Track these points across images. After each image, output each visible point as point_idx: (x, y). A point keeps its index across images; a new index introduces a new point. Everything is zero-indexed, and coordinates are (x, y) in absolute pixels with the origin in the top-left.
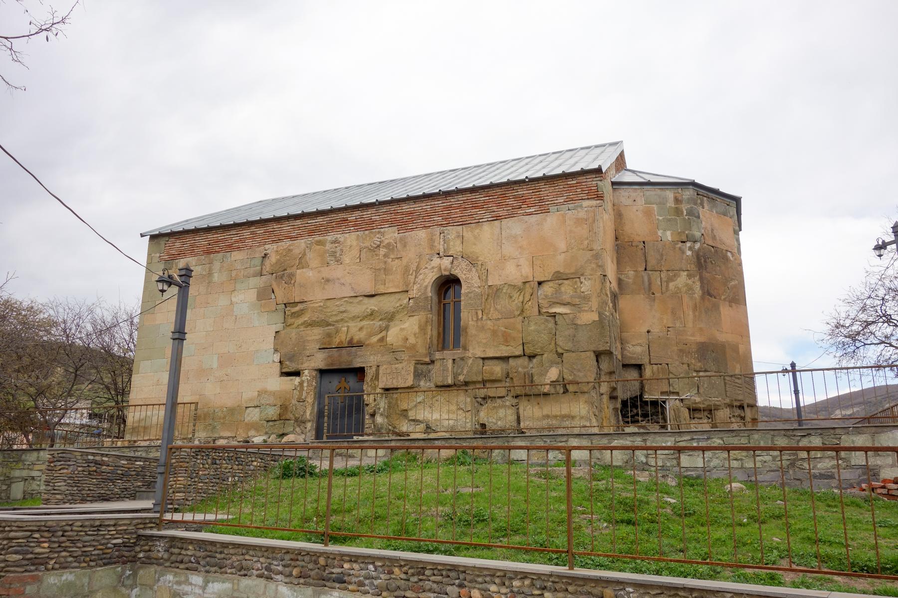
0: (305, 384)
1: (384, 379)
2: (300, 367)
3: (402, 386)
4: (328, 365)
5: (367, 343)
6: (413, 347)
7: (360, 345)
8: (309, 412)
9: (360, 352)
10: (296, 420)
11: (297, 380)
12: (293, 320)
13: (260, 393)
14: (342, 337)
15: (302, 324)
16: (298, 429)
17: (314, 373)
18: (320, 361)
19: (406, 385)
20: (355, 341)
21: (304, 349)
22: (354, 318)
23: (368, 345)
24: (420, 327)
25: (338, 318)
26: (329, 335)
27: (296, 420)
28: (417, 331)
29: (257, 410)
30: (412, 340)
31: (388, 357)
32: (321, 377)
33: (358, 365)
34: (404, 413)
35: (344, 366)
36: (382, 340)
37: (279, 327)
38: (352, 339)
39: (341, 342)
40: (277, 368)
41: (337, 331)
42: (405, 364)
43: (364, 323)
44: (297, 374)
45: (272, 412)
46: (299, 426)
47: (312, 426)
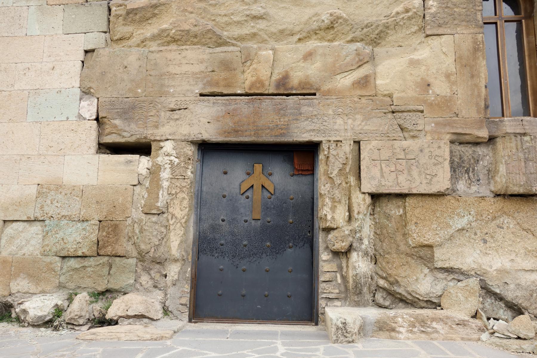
0: (165, 174)
1: (376, 172)
3: (423, 190)
4: (228, 133)
5: (326, 87)
6: (445, 103)
7: (308, 93)
8: (178, 240)
9: (308, 107)
10: (142, 257)
11: (143, 163)
12: (129, 29)
13: (43, 190)
14: (262, 70)
15: (154, 38)
16: (144, 279)
17: (190, 150)
18: (206, 122)
19: (433, 190)
21: (163, 94)
22: (283, 34)
23: (328, 93)
24: (458, 59)
25: (245, 31)
26: (226, 65)
27: (142, 257)
28: (453, 69)
29: (36, 228)
30: (440, 88)
31: (385, 123)
33: (305, 137)
34: (424, 254)
35: (267, 138)
36: (365, 82)
37: (95, 40)
40: (89, 134)
41: (248, 58)
42: (424, 141)
43: (312, 44)
44: (143, 149)
45: (77, 237)
46: (147, 270)
47: (181, 272)
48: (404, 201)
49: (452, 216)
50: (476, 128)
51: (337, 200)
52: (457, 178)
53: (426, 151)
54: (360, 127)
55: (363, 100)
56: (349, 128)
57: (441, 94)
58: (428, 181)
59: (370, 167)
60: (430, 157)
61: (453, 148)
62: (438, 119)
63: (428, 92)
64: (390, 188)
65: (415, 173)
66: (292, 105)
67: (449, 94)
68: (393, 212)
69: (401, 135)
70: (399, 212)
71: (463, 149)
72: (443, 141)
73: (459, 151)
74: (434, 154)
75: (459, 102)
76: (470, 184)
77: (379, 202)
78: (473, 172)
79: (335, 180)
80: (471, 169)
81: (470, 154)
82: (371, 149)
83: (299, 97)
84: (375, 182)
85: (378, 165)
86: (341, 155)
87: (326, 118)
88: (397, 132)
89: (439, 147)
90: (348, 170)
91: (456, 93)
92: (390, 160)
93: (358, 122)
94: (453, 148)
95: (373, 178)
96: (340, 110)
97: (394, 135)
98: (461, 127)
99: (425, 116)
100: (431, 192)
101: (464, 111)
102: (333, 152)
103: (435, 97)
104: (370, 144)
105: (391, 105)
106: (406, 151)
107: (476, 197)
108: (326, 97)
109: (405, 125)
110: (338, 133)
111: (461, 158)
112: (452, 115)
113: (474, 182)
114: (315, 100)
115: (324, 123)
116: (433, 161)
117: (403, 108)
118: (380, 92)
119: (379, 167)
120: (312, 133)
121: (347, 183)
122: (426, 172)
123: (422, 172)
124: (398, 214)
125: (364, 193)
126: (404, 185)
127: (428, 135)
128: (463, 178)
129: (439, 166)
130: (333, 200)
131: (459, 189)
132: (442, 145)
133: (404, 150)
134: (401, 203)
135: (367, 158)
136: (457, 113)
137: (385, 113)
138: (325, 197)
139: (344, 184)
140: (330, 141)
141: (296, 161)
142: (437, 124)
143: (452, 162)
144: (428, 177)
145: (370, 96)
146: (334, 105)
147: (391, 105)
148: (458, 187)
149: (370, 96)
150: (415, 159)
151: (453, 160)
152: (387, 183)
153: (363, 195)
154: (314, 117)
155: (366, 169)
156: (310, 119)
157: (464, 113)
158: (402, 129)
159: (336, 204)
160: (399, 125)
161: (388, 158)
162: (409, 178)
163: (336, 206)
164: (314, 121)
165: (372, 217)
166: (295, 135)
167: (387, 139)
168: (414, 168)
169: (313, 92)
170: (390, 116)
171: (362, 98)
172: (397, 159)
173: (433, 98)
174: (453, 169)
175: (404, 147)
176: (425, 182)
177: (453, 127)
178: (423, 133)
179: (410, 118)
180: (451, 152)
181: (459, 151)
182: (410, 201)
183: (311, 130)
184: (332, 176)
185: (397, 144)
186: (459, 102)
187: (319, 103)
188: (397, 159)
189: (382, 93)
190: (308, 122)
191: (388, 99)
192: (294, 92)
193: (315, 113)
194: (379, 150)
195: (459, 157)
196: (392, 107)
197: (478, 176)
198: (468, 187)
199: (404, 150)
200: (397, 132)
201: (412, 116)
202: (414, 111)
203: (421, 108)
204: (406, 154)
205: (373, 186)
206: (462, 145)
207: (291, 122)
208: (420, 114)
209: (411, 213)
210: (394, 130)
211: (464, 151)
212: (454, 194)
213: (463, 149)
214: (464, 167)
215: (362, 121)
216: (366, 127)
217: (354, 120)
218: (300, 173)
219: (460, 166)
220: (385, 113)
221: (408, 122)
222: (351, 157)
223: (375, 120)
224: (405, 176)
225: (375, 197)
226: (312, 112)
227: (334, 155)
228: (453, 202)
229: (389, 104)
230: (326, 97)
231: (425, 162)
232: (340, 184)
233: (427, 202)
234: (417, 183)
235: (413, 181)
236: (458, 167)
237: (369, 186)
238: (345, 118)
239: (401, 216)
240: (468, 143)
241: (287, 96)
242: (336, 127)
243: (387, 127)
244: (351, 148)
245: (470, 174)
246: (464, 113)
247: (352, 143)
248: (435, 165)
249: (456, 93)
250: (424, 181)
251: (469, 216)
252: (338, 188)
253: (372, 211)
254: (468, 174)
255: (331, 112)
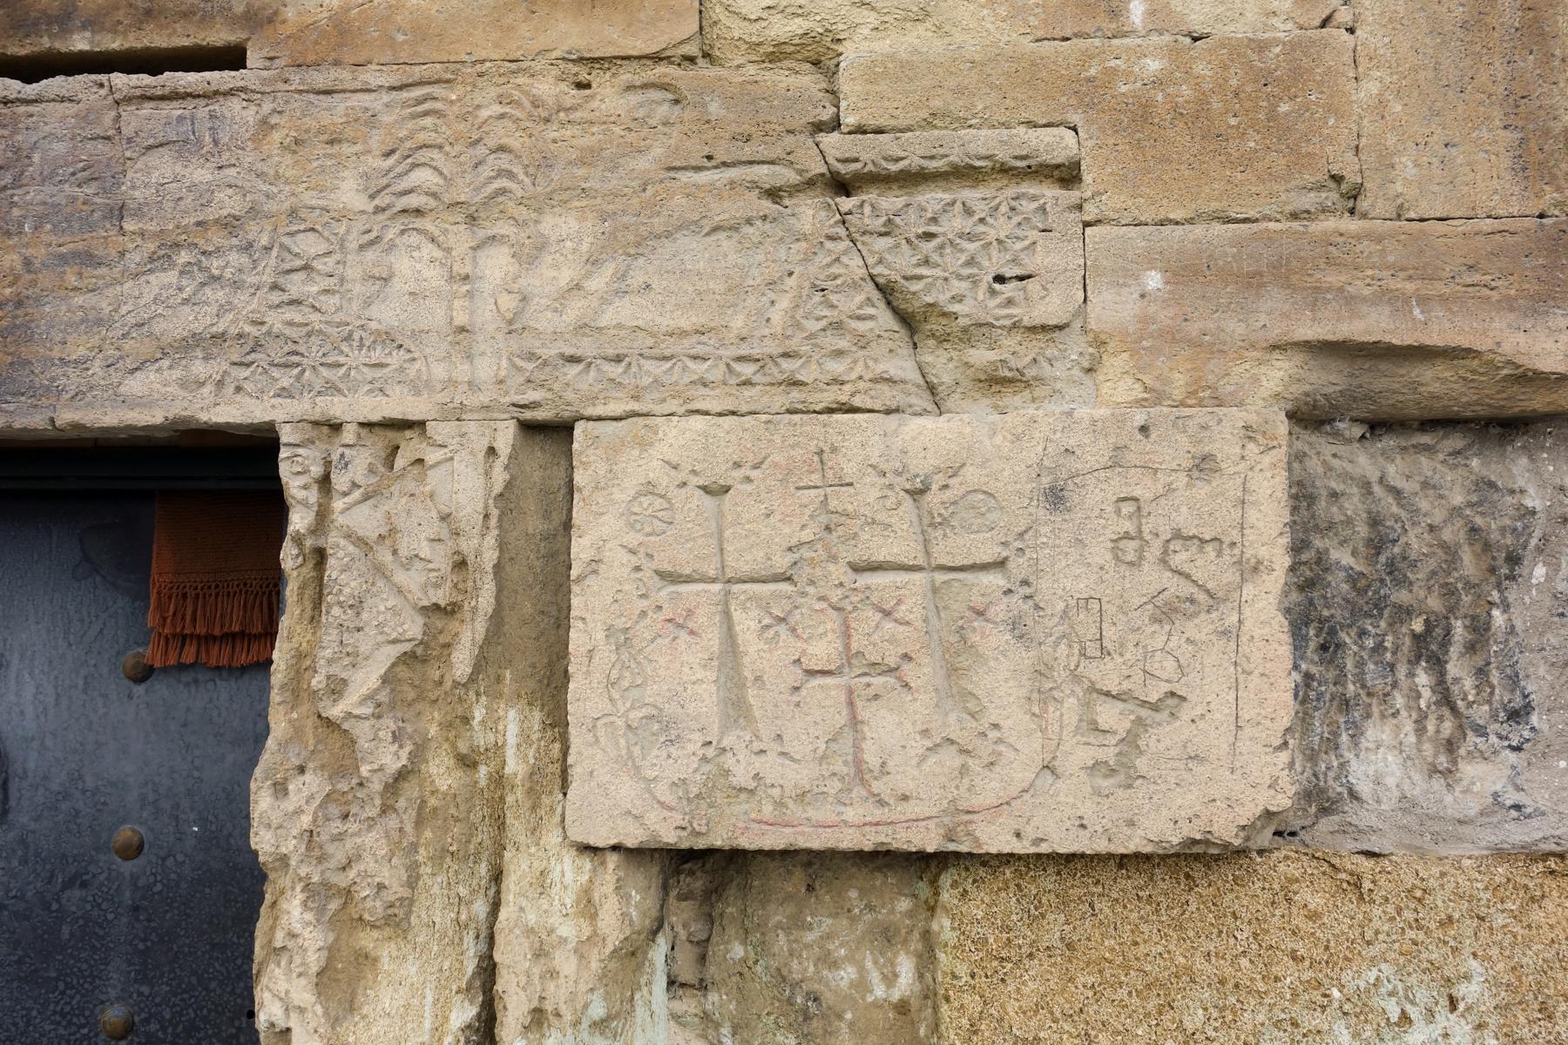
1: (684, 674)
19: (1157, 828)
42: (1083, 409)
48: (923, 889)
49: (1311, 1021)
50: (1509, 304)
51: (376, 908)
52: (1345, 704)
53: (1097, 496)
54: (575, 310)
55: (608, 96)
56: (486, 316)
57: (1220, 31)
58: (1109, 754)
59: (643, 631)
60: (1129, 549)
61: (1314, 465)
62: (1198, 230)
63: (1114, 14)
64: (795, 811)
65: (1001, 679)
66: (60, 148)
67: (1283, 29)
68: (848, 974)
69: (902, 365)
70: (890, 979)
71: (1395, 471)
72: (1238, 416)
73: (1366, 486)
74: (1158, 523)
75: (1370, 87)
76: (1450, 746)
77: (745, 889)
78: (1471, 648)
79: (364, 744)
80: (1459, 628)
81: (1456, 511)
82: (650, 489)
83: (119, 79)
84: (677, 765)
85: (701, 619)
86: (419, 536)
87: (309, 245)
88: (862, 342)
89: (1204, 465)
90: (462, 662)
91: (1344, 15)
92: (802, 574)
93: (556, 273)
94: (1314, 465)
95: (663, 727)
96: (422, 177)
97: (837, 367)
98: (1385, 296)
99: (1091, 212)
100: (1133, 843)
101: (1406, 166)
102: (360, 518)
103: (1174, 52)
104: (644, 445)
105: (818, 127)
106: (933, 498)
107: (1500, 854)
108: (320, 79)
109: (922, 293)
110: (397, 358)
111: (1377, 544)
112: (1308, 201)
113: (1481, 731)
114: (235, 104)
115: (297, 285)
116: (1152, 578)
117: (912, 151)
118: (738, 29)
119: (712, 639)
120: (199, 368)
121: (467, 762)
122: (1092, 671)
123: (1060, 675)
124: (879, 991)
125: (588, 849)
126: (906, 784)
127: (1115, 363)
128: (1399, 700)
129: (1201, 627)
130: (337, 904)
131: (1364, 788)
132: (1225, 444)
133: (917, 493)
134: (904, 904)
135: (618, 562)
136: (1352, 178)
137: (773, 194)
138: (285, 882)
139: (441, 773)
140: (336, 427)
141: (161, 572)
142: (1187, 273)
143: (1308, 577)
144: (1110, 715)
145: (657, 58)
146: (377, 140)
147: (818, 127)
148: (1360, 773)
149: (657, 58)
150: (1001, 564)
151: (1321, 559)
152: (771, 767)
153: (587, 863)
154: (217, 238)
155: (605, 655)
156: (184, 257)
157: (1408, 178)
158: (908, 321)
159: (367, 940)
160: (886, 291)
161: (781, 562)
162: (954, 724)
163: (365, 960)
164: (215, 264)
165: (688, 1005)
166: (72, 380)
167: (780, 400)
168: (993, 639)
169: (219, 36)
170: (810, 213)
171: (597, 78)
172: (857, 569)
173: (1153, 65)
174: (1316, 624)
175: (921, 465)
176: (1086, 755)
177: (1316, 297)
178: (1075, 346)
179: (968, 225)
180: (1302, 496)
181: (1366, 486)
182: (965, 911)
183: (191, 344)
184: (335, 711)
185: (861, 441)
186: (1370, 87)
187: (265, 126)
188: (857, 569)
189: (751, 32)
190: (171, 277)
191: (809, 81)
192: (80, 43)
193: (229, 203)
194: (717, 491)
195: (1363, 530)
196: (830, 140)
197: (1514, 681)
198: (1434, 770)
199: (917, 493)
200: (862, 342)
201: (981, 209)
202: (1004, 170)
203: (1057, 145)
204: (932, 524)
205: (663, 792)
206: (1389, 442)
207: (46, 279)
208: (1049, 192)
209: (972, 1003)
210: (837, 326)
211: (1408, 487)
212: (1326, 824)
213: (1395, 471)
214: (1404, 613)
215: (594, 262)
216: (623, 312)
217: (531, 254)
218: (189, 655)
219: (1368, 600)
220: (773, 194)
221: (955, 261)
222: (490, 556)
223: (693, 250)
224: (920, 707)
225: (703, 878)
226: (204, 196)
227: (361, 542)
228: (1316, 901)
229: (799, 122)
230: (320, 79)
231: (1082, 587)
232: (402, 776)
233: (1102, 906)
234: (1019, 770)
235: (984, 749)
236: (1355, 612)
237: (628, 790)
238: (460, 238)
239: (902, 1008)
240: (1440, 423)
241: (28, 80)
242: (386, 314)
243: (784, 303)
244: (500, 477)
245: (1453, 669)
246: (1408, 178)
247: (506, 436)
248: (1166, 612)
249: (1344, 15)
250: (1078, 755)
251: (1444, 1019)
252: (385, 810)
253: (686, 956)
254: (1438, 664)
255: (349, 194)
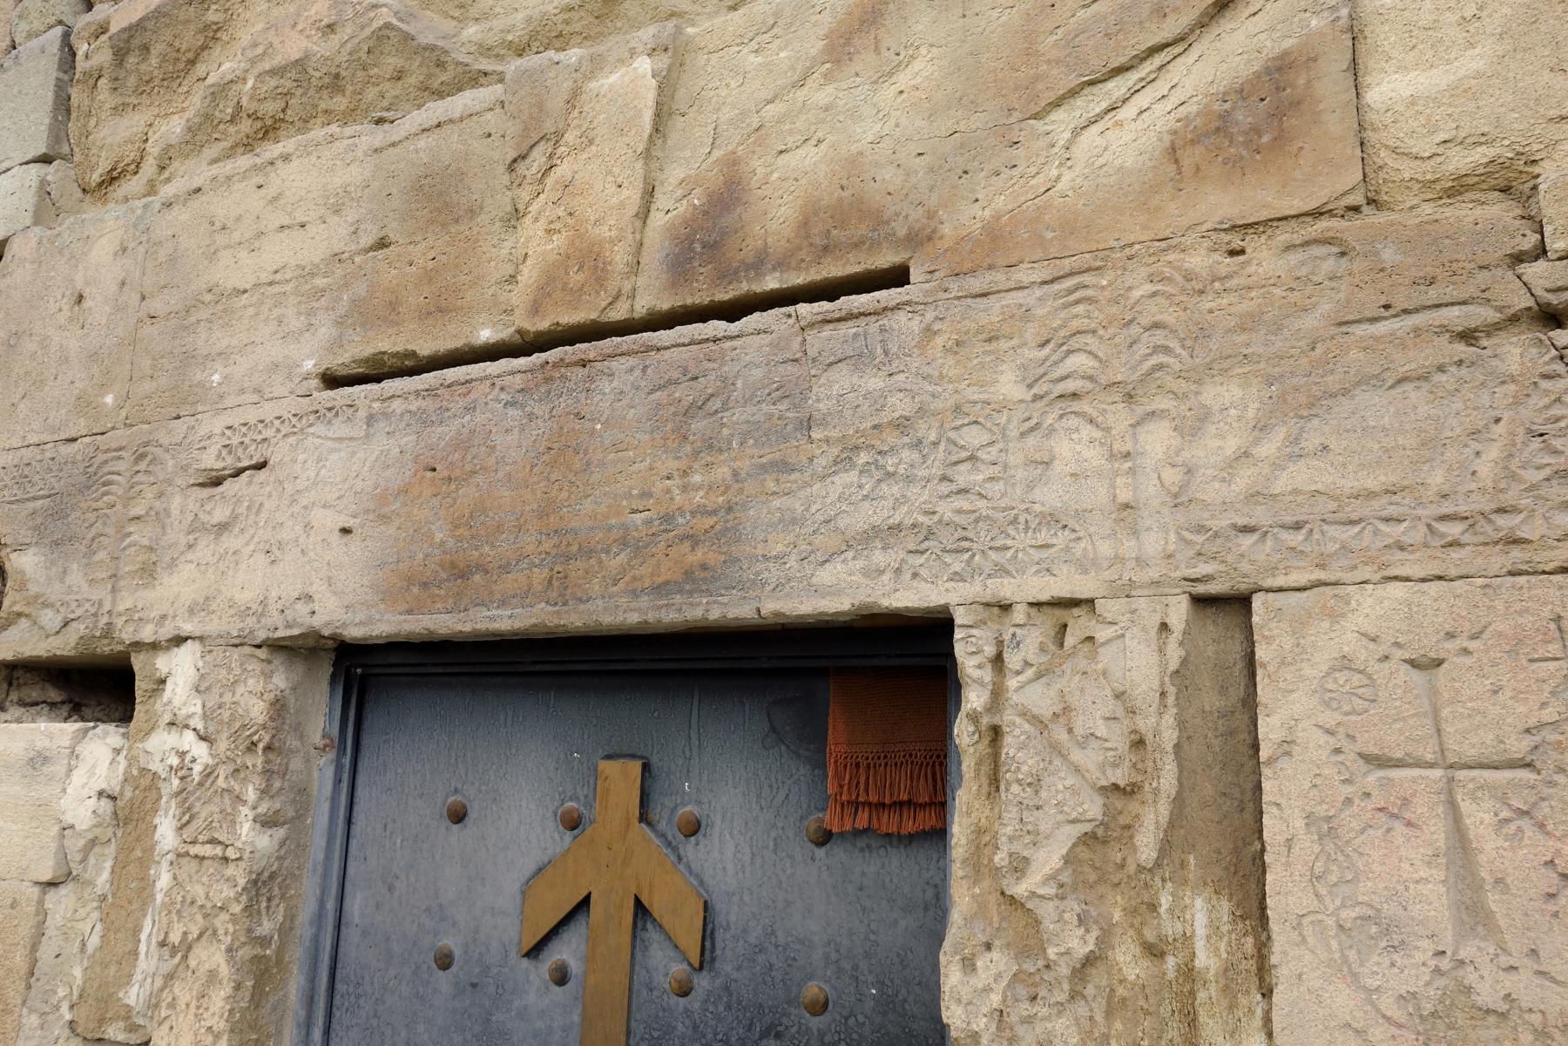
2: (133, 611)
5: (965, 218)
9: (847, 369)
11: (94, 755)
12: (132, 124)
18: (316, 534)
20: (774, 215)
21: (185, 401)
23: (994, 246)
32: (352, 742)
33: (833, 588)
38: (727, 197)
39: (588, 258)
